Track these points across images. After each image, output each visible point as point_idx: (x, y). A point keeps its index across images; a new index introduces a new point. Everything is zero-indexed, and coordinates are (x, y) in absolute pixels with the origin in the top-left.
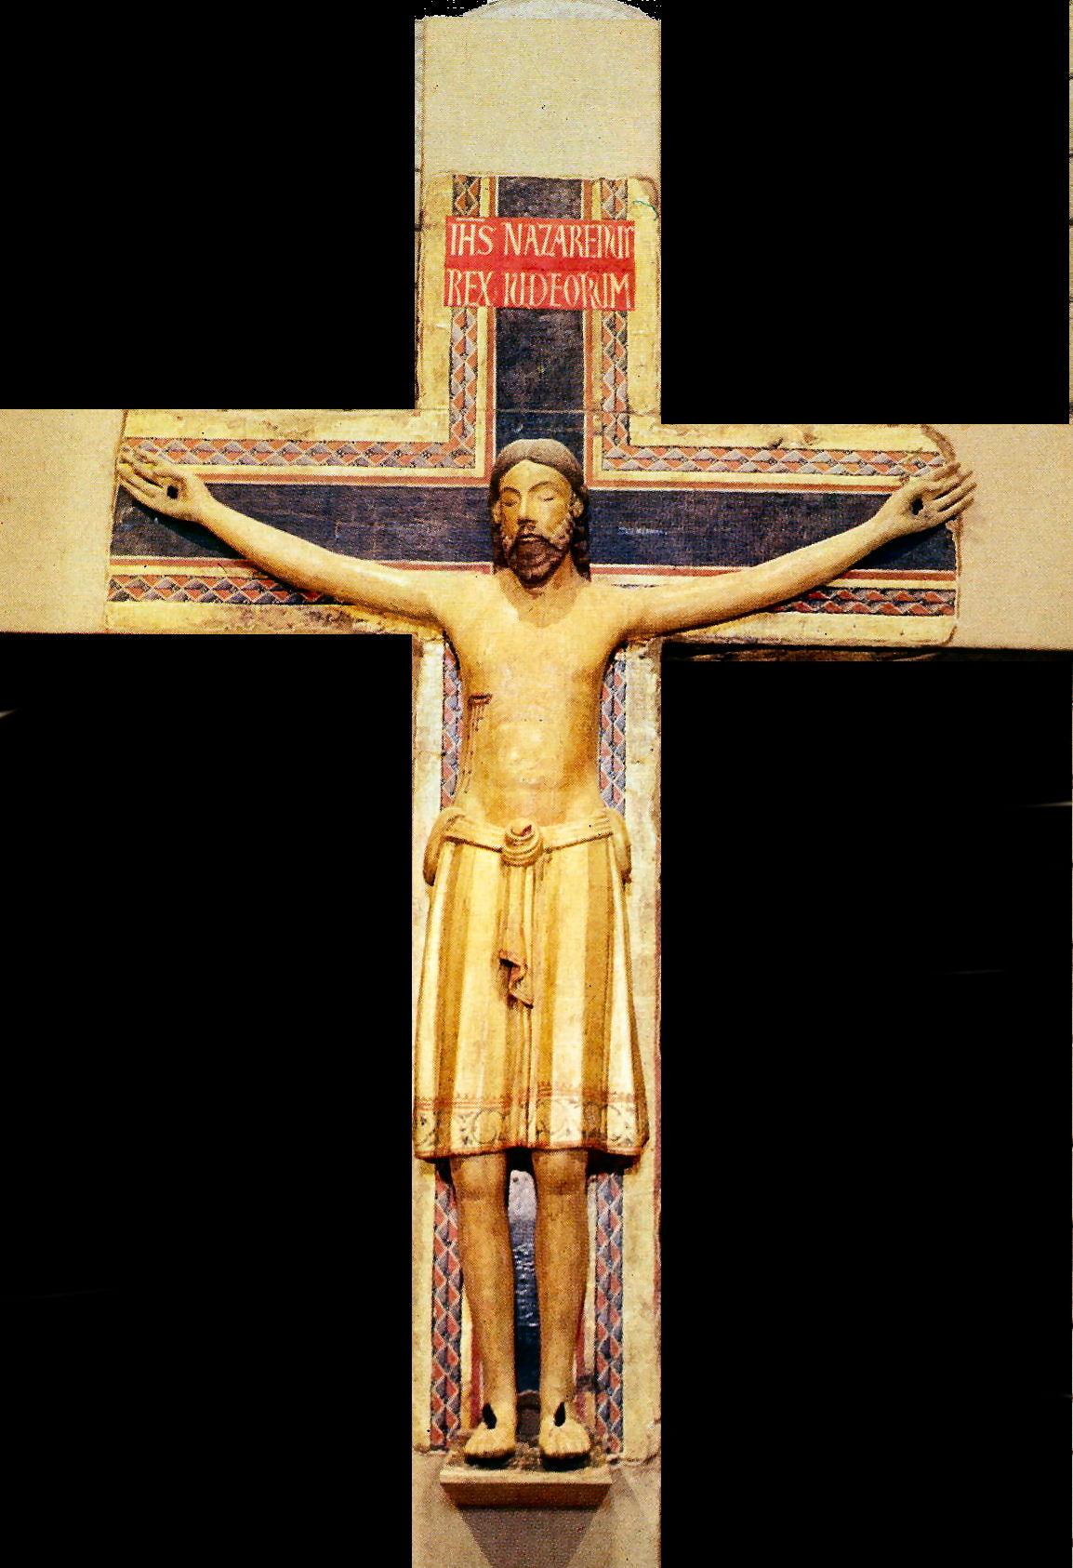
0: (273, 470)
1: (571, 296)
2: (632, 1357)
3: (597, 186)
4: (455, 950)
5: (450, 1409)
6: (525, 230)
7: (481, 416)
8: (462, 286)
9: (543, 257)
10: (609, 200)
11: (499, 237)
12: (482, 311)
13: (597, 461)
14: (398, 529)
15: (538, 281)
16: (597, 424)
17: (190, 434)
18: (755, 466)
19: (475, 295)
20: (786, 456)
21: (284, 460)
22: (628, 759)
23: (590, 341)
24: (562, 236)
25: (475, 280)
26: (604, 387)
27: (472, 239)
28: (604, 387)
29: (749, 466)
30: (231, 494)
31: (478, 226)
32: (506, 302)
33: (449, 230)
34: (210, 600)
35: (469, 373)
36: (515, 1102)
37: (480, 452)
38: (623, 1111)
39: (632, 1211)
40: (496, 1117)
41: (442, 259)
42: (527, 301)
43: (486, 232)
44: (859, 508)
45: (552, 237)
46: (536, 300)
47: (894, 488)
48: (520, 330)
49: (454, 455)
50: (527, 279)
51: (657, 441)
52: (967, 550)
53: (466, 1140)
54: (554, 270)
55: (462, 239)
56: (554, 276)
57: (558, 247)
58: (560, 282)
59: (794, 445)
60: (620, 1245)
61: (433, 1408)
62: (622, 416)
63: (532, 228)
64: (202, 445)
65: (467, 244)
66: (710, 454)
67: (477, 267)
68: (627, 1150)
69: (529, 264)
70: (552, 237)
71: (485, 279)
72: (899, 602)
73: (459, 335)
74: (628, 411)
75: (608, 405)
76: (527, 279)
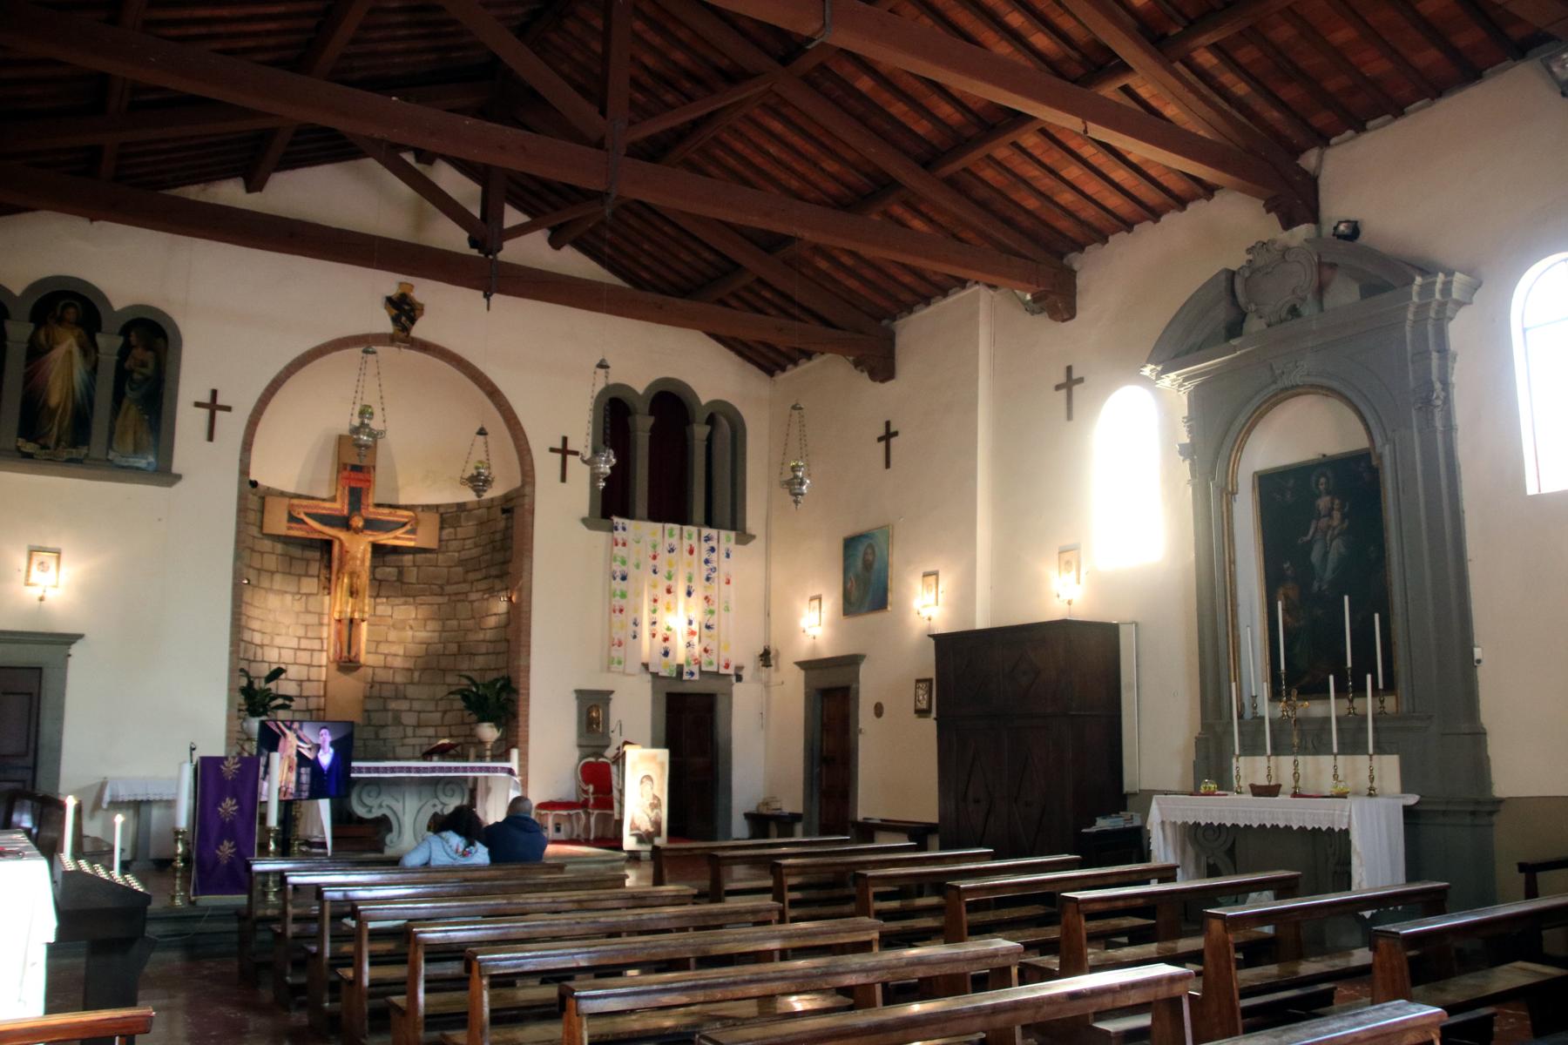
24: (361, 476)
30: (307, 514)
44: (404, 524)
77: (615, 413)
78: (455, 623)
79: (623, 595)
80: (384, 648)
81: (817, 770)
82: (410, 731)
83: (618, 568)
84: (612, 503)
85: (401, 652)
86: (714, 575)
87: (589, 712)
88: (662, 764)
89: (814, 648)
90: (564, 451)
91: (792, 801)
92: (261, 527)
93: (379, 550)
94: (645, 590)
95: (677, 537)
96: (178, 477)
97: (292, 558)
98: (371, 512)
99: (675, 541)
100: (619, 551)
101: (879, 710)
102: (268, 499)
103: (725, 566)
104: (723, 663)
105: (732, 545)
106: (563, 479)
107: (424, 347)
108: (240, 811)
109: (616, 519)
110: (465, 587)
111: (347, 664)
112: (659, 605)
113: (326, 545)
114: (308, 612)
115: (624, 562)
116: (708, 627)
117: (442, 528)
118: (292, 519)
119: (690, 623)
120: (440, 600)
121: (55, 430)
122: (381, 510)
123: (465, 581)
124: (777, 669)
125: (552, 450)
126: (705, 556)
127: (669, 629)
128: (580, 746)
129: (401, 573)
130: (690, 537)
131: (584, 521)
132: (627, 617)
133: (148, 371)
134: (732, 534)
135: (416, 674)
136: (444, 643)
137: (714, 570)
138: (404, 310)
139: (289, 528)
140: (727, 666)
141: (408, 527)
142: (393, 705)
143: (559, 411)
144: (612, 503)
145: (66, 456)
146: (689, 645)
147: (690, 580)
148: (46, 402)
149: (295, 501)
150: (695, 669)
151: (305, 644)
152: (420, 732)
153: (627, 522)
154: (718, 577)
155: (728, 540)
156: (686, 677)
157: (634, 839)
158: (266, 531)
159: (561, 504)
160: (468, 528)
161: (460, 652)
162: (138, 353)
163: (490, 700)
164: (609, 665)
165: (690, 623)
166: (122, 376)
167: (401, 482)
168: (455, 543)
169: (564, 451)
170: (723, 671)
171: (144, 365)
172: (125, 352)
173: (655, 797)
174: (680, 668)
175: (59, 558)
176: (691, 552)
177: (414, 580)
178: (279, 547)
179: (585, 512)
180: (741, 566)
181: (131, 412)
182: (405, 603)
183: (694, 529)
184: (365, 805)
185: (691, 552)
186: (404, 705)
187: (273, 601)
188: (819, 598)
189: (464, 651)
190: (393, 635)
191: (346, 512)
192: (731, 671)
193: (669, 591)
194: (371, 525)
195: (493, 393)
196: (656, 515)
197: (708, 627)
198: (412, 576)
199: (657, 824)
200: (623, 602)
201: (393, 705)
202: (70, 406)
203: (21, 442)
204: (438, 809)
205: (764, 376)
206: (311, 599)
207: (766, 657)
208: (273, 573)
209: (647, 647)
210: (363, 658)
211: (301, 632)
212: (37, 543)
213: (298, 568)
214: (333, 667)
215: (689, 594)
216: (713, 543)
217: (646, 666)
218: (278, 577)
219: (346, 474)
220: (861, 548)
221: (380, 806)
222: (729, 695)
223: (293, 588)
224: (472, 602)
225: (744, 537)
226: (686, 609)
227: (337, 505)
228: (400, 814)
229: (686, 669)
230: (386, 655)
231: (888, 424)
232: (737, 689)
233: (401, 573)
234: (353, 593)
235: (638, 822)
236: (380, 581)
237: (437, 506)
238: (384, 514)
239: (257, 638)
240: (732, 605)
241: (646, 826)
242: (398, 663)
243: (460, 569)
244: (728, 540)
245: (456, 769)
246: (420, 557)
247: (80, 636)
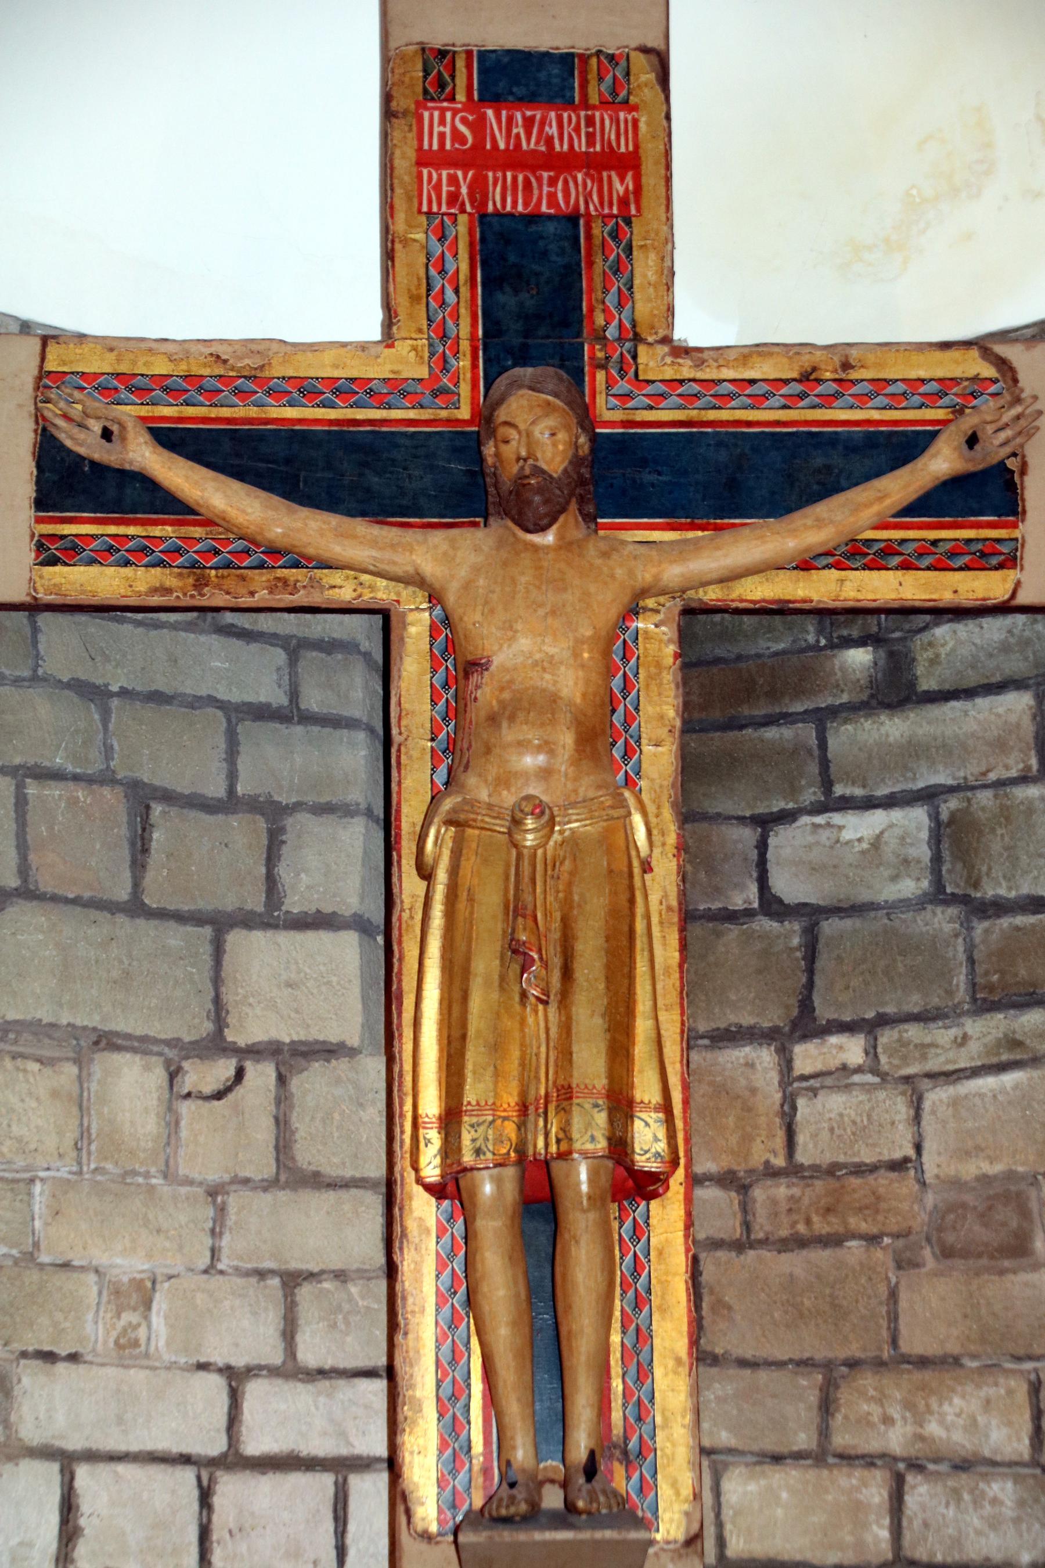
0: (225, 412)
1: (567, 203)
2: (665, 1419)
3: (594, 61)
4: (461, 945)
5: (459, 1488)
6: (510, 119)
7: (465, 346)
8: (438, 187)
9: (534, 151)
10: (609, 78)
11: (479, 126)
12: (463, 219)
13: (601, 400)
14: (374, 480)
15: (527, 184)
16: (600, 355)
17: (123, 368)
18: (783, 401)
19: (454, 198)
20: (820, 389)
21: (235, 400)
22: (644, 741)
23: (589, 254)
24: (559, 129)
25: (453, 180)
26: (606, 310)
27: (448, 130)
28: (606, 310)
29: (675, 400)
30: (170, 439)
31: (455, 112)
32: (490, 208)
33: (420, 119)
34: (154, 566)
35: (450, 296)
36: (532, 1109)
37: (465, 389)
38: (650, 1121)
39: (660, 1253)
40: (510, 1129)
41: (412, 155)
42: (515, 203)
43: (464, 121)
44: (904, 447)
45: (543, 123)
46: (526, 204)
47: (945, 423)
48: (508, 242)
49: (435, 394)
50: (515, 179)
51: (669, 374)
52: (1035, 490)
53: (478, 1152)
54: (548, 169)
55: (436, 129)
56: (545, 175)
57: (549, 141)
58: (553, 182)
59: (828, 375)
60: (649, 1291)
61: (441, 1483)
62: (628, 345)
63: (518, 116)
64: (138, 381)
65: (442, 136)
66: (730, 387)
67: (455, 165)
68: (653, 1166)
69: (515, 160)
70: (543, 123)
71: (464, 180)
72: (953, 554)
73: (437, 249)
74: (637, 338)
75: (612, 333)
76: (515, 179)
139: (50, 552)
151: (275, 1418)
194: (642, 476)
211: (247, 1332)
219: (444, 125)
230: (900, 1472)
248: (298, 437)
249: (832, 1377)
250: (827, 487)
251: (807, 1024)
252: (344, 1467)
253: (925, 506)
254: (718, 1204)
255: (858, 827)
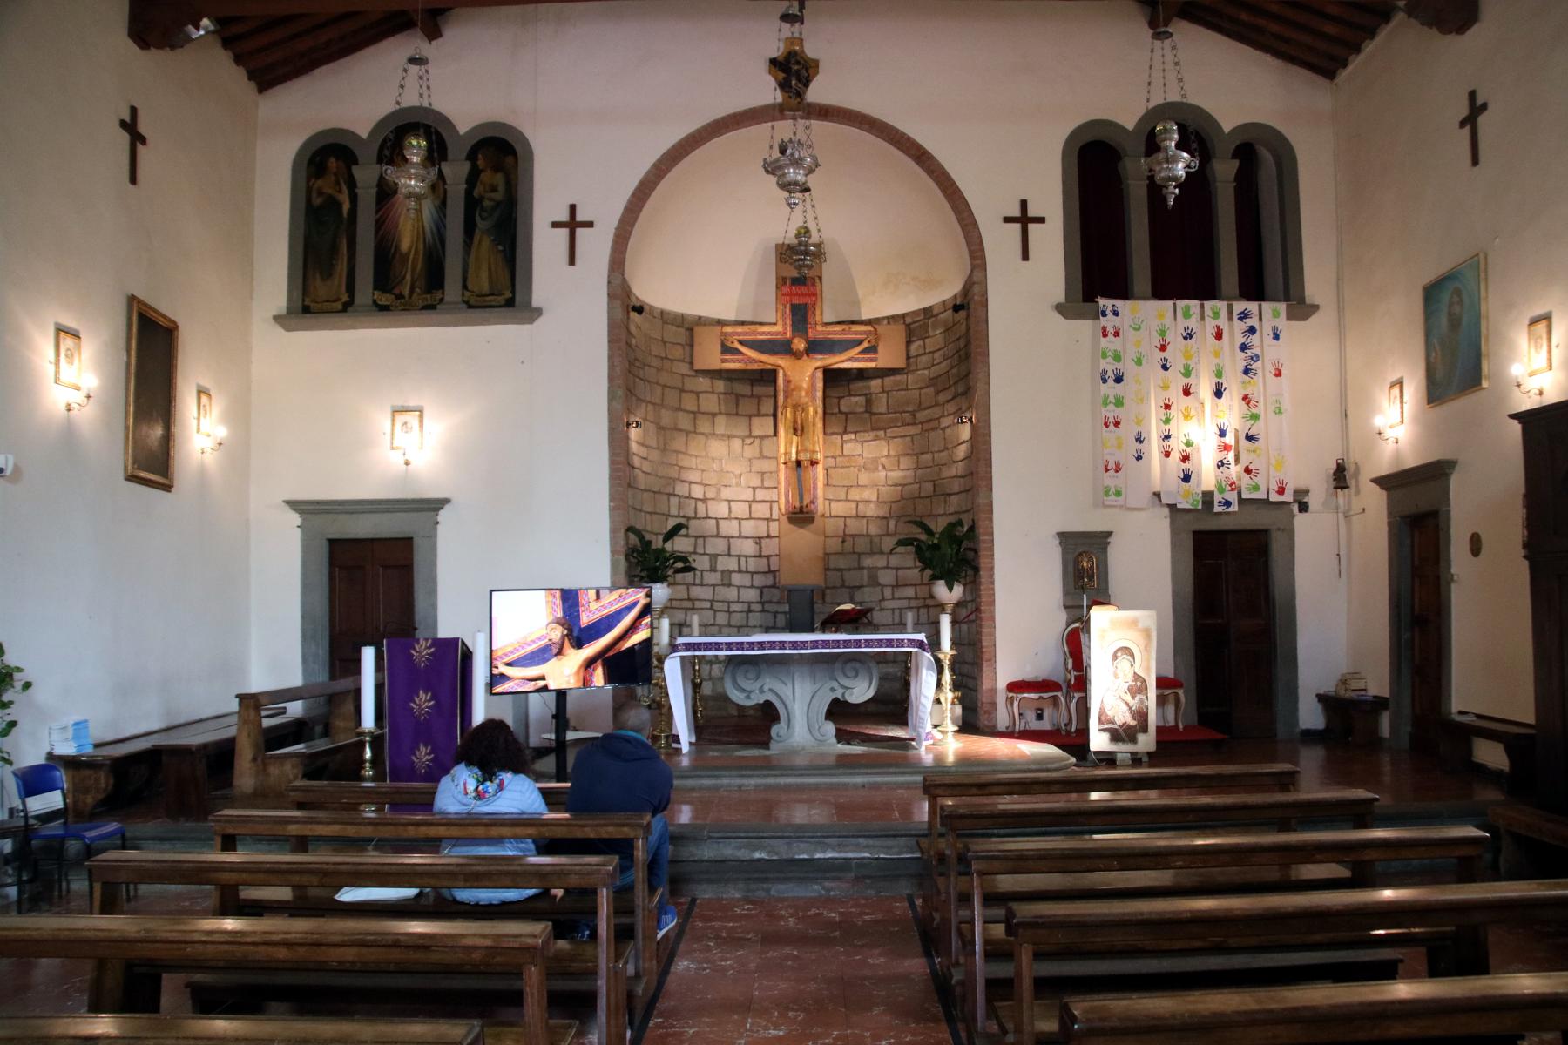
24: (804, 290)
30: (741, 343)
44: (861, 342)
77: (1096, 162)
78: (928, 457)
79: (1119, 402)
80: (855, 494)
81: (1406, 636)
82: (888, 592)
83: (1110, 366)
84: (1098, 276)
85: (874, 498)
86: (1254, 366)
87: (1077, 562)
88: (1147, 632)
89: (1397, 455)
90: (1024, 219)
91: (1377, 683)
92: (691, 363)
93: (833, 378)
94: (1150, 392)
95: (1196, 317)
96: (538, 312)
97: (738, 396)
98: (818, 332)
99: (1193, 323)
100: (1110, 343)
101: (1476, 545)
102: (698, 330)
103: (1271, 352)
104: (1274, 486)
105: (1282, 323)
106: (1025, 257)
107: (825, 113)
108: (437, 707)
109: (1102, 301)
110: (936, 412)
111: (801, 516)
112: (1173, 412)
113: (767, 377)
114: (762, 456)
115: (1117, 358)
116: (1249, 438)
117: (909, 343)
118: (726, 350)
119: (1222, 433)
120: (912, 430)
121: (408, 277)
122: (830, 328)
123: (937, 404)
124: (1358, 492)
125: (1007, 220)
126: (1240, 340)
127: (1189, 444)
128: (1066, 607)
129: (869, 402)
130: (1216, 315)
131: (1060, 308)
132: (1127, 432)
133: (498, 196)
134: (1282, 307)
135: (892, 524)
136: (919, 482)
137: (1255, 358)
138: (793, 71)
139: (723, 361)
140: (1281, 491)
141: (865, 345)
142: (868, 562)
143: (1018, 170)
144: (1098, 276)
145: (421, 304)
146: (1221, 464)
147: (1219, 374)
148: (397, 247)
149: (728, 329)
150: (1232, 497)
151: (760, 495)
152: (899, 593)
153: (1119, 303)
154: (1263, 369)
155: (1276, 315)
156: (1217, 509)
157: (1106, 736)
158: (697, 367)
159: (1028, 286)
160: (936, 338)
161: (935, 494)
162: (486, 177)
163: (948, 545)
164: (1106, 496)
165: (1222, 433)
166: (472, 204)
167: (860, 293)
168: (924, 358)
169: (1024, 219)
170: (1274, 497)
171: (494, 189)
172: (473, 178)
173: (1137, 677)
174: (1208, 497)
175: (421, 417)
176: (1219, 336)
177: (884, 410)
178: (720, 385)
179: (1060, 295)
180: (1298, 351)
181: (484, 244)
182: (876, 438)
183: (1221, 305)
184: (743, 690)
185: (1219, 336)
186: (880, 561)
187: (717, 448)
188: (1400, 383)
189: (940, 493)
190: (864, 478)
191: (789, 335)
192: (1288, 497)
193: (1187, 393)
194: (815, 347)
195: (921, 157)
196: (1161, 292)
197: (1249, 438)
198: (881, 406)
199: (1141, 715)
200: (1119, 412)
201: (868, 562)
202: (421, 246)
203: (377, 294)
204: (838, 694)
205: (1320, 80)
206: (766, 442)
207: (1340, 477)
208: (714, 415)
209: (1159, 470)
210: (821, 507)
211: (756, 482)
212: (399, 403)
213: (747, 406)
214: (784, 519)
215: (1218, 394)
216: (1253, 321)
217: (1157, 495)
218: (721, 420)
219: (785, 290)
220: (1445, 297)
221: (762, 691)
222: (1290, 532)
223: (742, 430)
224: (944, 429)
225: (1301, 309)
226: (1214, 415)
227: (779, 328)
228: (789, 704)
229: (1217, 498)
230: (858, 502)
231: (1472, 95)
232: (1300, 520)
233: (869, 402)
234: (798, 429)
235: (1110, 713)
236: (846, 414)
237: (904, 316)
238: (836, 333)
239: (697, 492)
240: (1286, 405)
241: (1122, 716)
242: (871, 510)
243: (931, 390)
244: (1276, 315)
245: (847, 643)
246: (888, 380)
247: (447, 501)
248: (763, 342)
249: (849, 487)
250: (847, 349)
251: (845, 432)
252: (772, 502)
253: (865, 351)
254: (831, 462)
255: (854, 399)
